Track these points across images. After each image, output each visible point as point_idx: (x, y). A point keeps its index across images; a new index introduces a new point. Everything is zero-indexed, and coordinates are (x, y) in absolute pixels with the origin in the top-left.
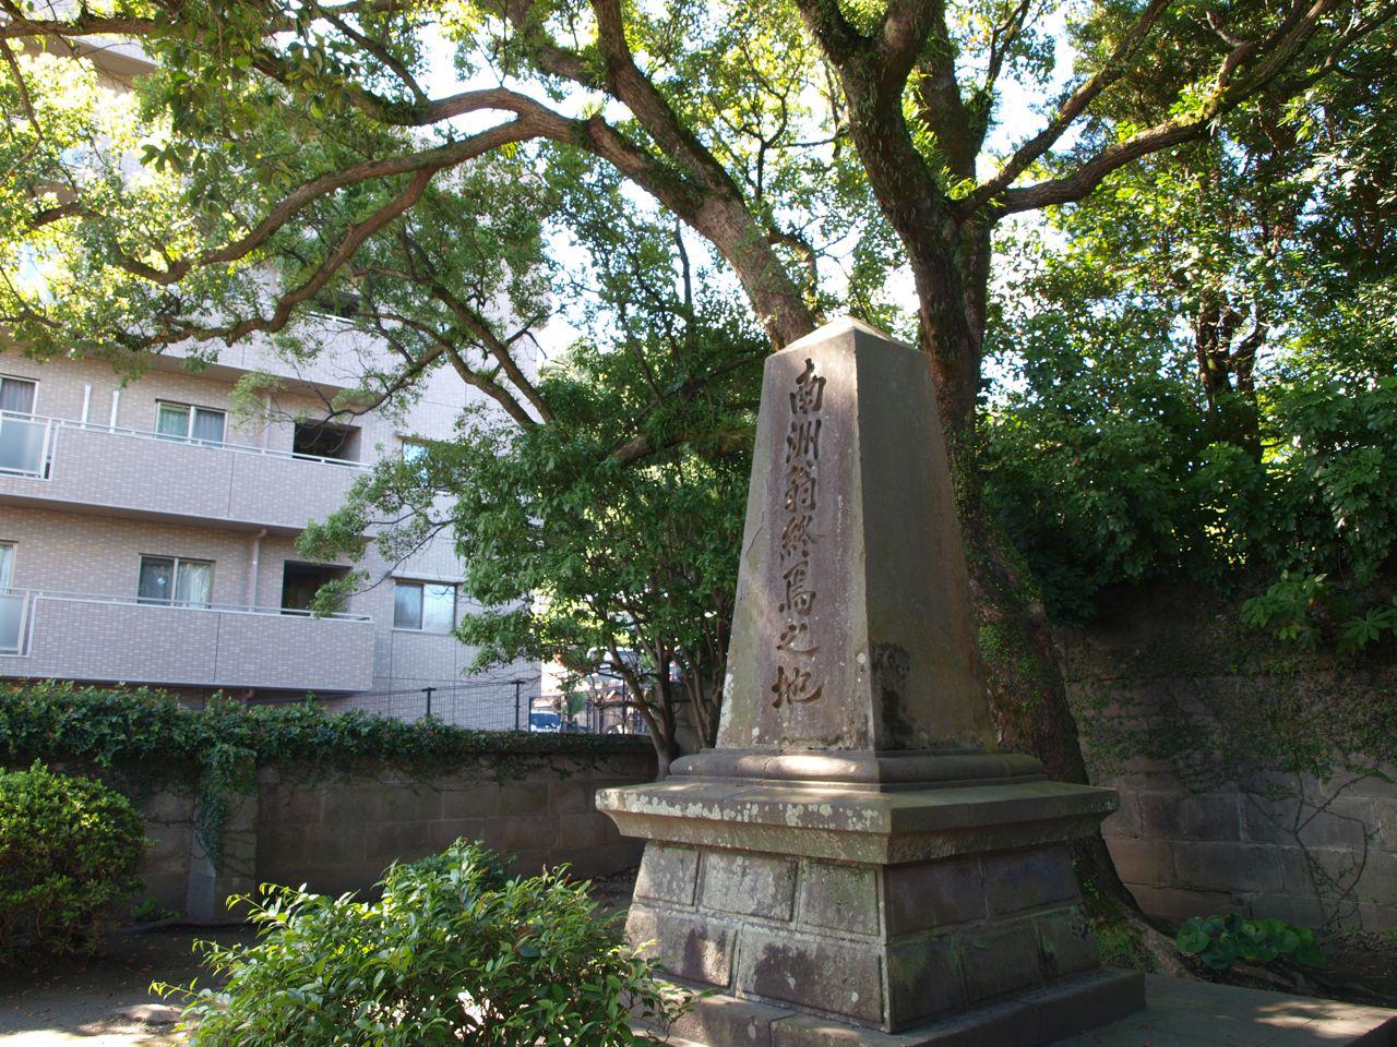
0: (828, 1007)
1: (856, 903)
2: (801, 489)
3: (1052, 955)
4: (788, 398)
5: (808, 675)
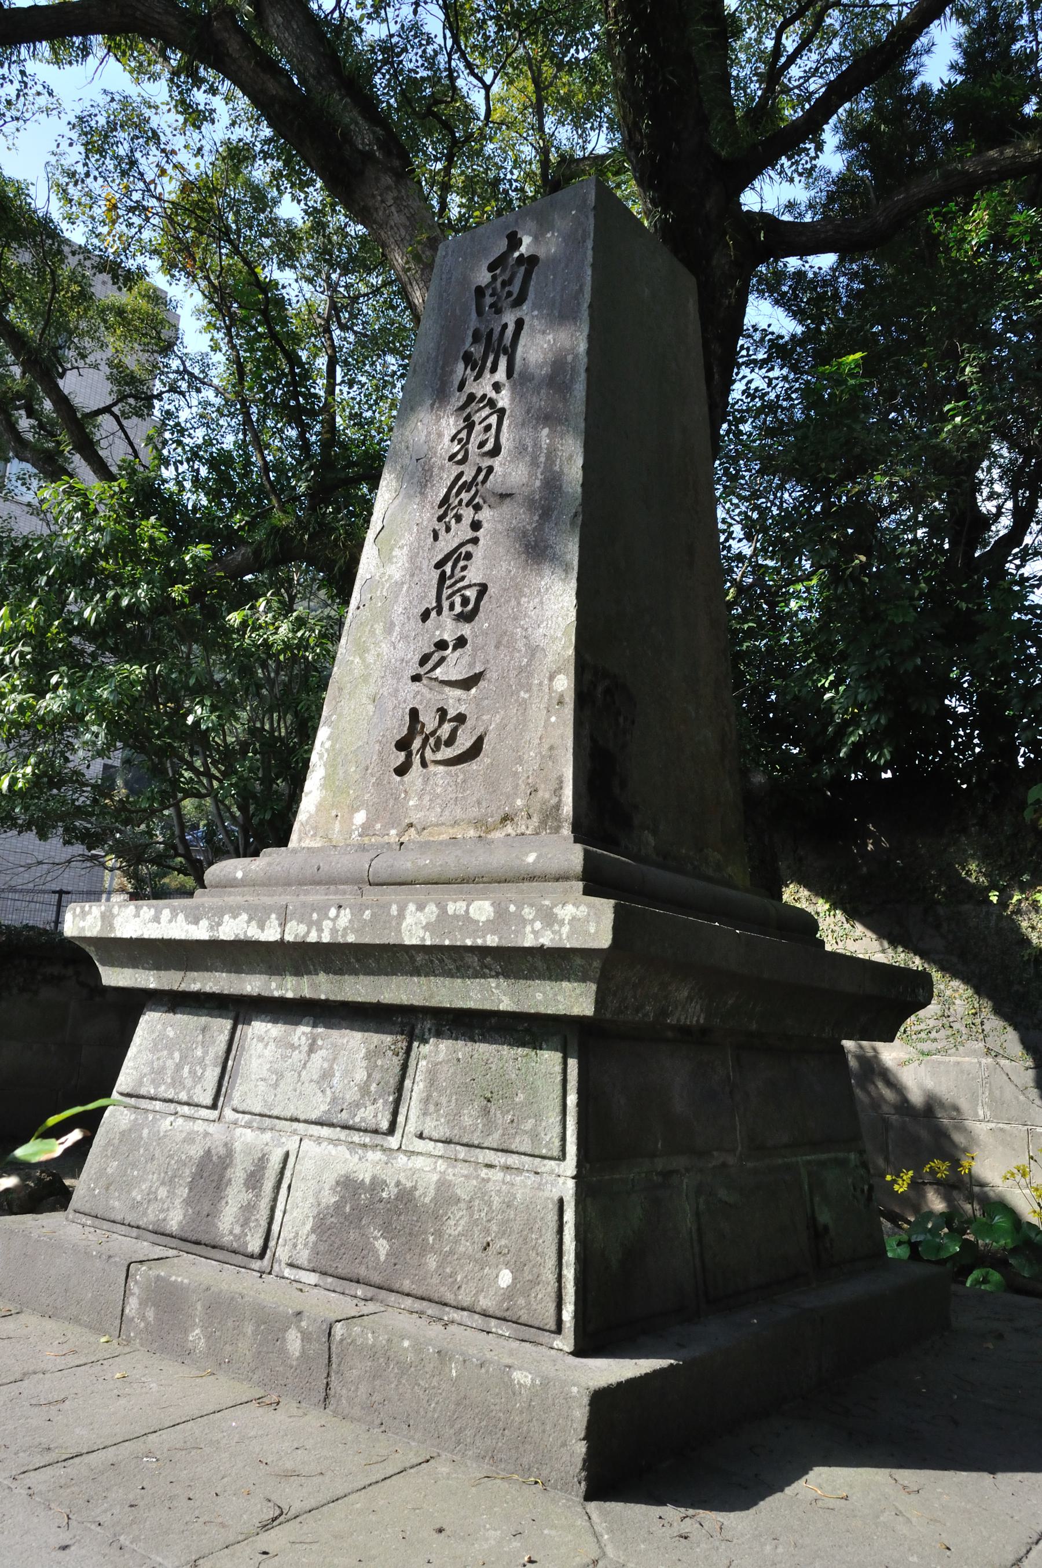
0: (449, 1297)
1: (521, 1098)
2: (478, 428)
3: (826, 1228)
5: (461, 718)
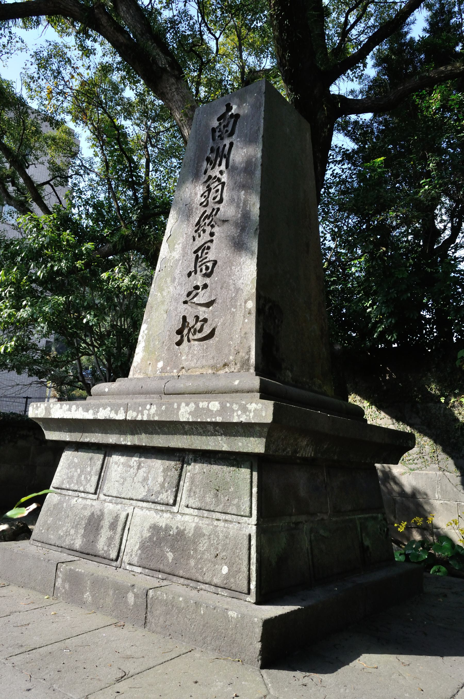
1: (232, 489)
3: (368, 547)
4: (210, 131)
5: (205, 320)
